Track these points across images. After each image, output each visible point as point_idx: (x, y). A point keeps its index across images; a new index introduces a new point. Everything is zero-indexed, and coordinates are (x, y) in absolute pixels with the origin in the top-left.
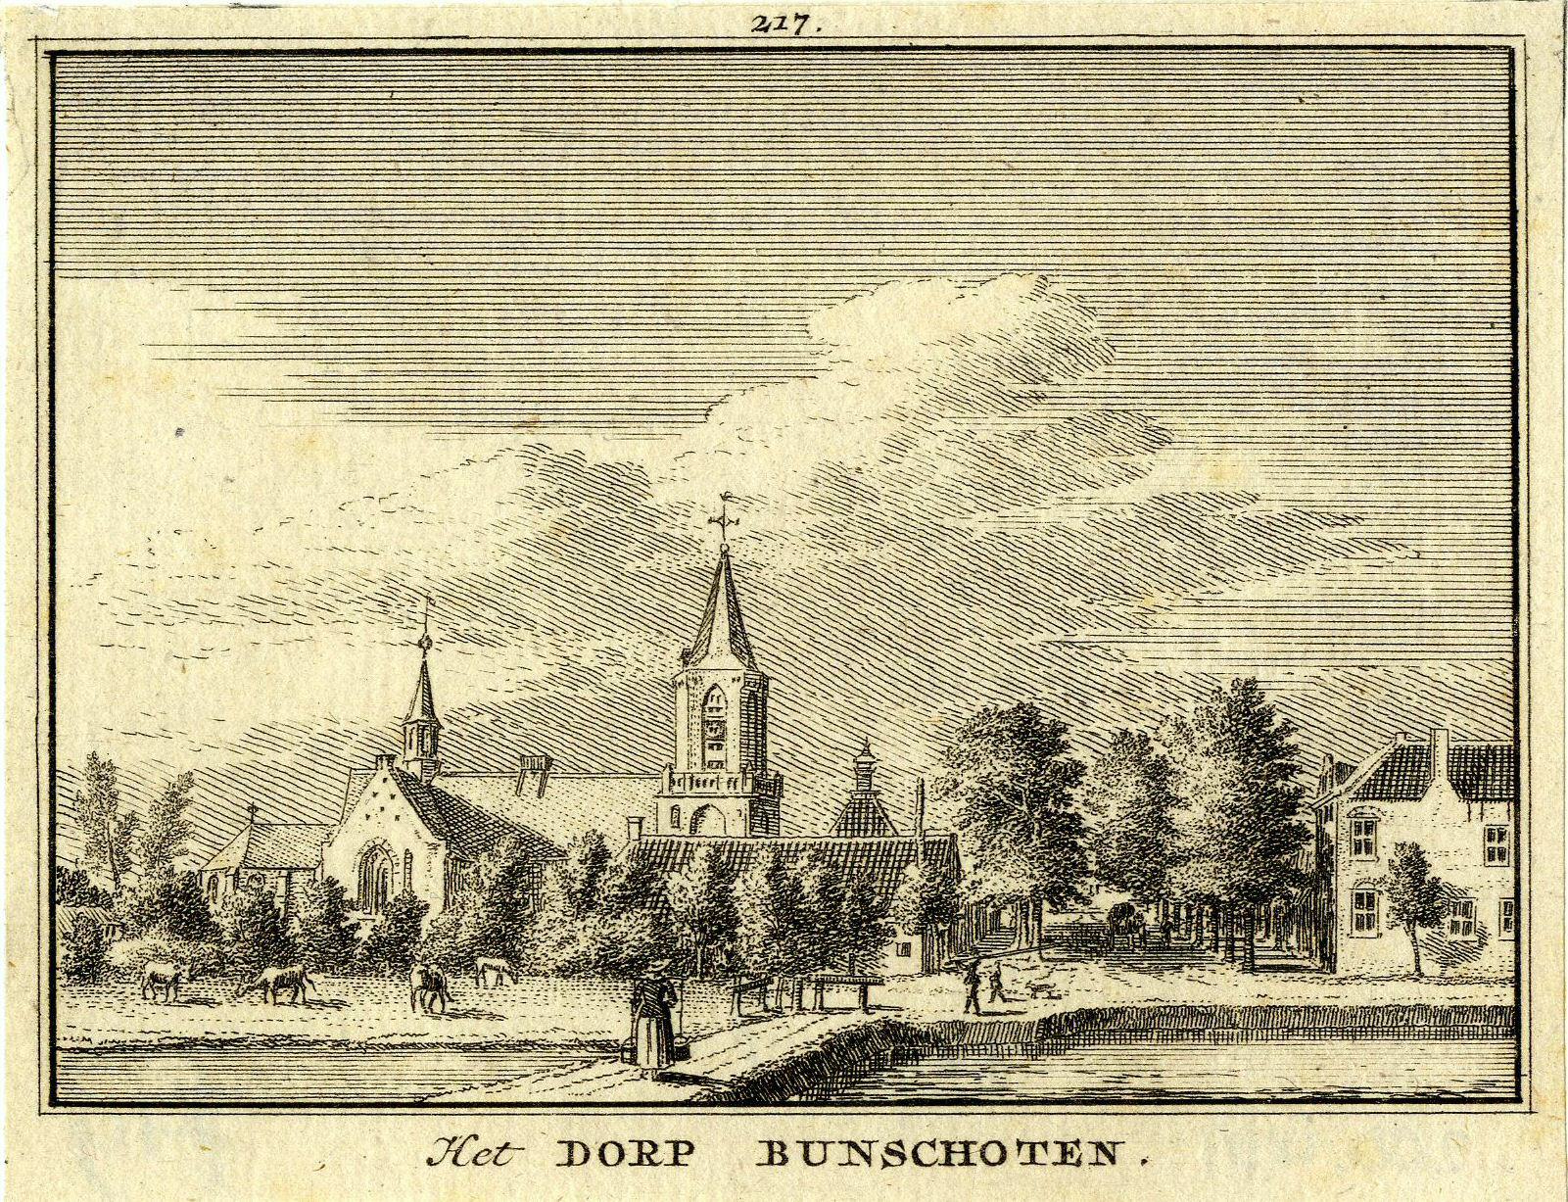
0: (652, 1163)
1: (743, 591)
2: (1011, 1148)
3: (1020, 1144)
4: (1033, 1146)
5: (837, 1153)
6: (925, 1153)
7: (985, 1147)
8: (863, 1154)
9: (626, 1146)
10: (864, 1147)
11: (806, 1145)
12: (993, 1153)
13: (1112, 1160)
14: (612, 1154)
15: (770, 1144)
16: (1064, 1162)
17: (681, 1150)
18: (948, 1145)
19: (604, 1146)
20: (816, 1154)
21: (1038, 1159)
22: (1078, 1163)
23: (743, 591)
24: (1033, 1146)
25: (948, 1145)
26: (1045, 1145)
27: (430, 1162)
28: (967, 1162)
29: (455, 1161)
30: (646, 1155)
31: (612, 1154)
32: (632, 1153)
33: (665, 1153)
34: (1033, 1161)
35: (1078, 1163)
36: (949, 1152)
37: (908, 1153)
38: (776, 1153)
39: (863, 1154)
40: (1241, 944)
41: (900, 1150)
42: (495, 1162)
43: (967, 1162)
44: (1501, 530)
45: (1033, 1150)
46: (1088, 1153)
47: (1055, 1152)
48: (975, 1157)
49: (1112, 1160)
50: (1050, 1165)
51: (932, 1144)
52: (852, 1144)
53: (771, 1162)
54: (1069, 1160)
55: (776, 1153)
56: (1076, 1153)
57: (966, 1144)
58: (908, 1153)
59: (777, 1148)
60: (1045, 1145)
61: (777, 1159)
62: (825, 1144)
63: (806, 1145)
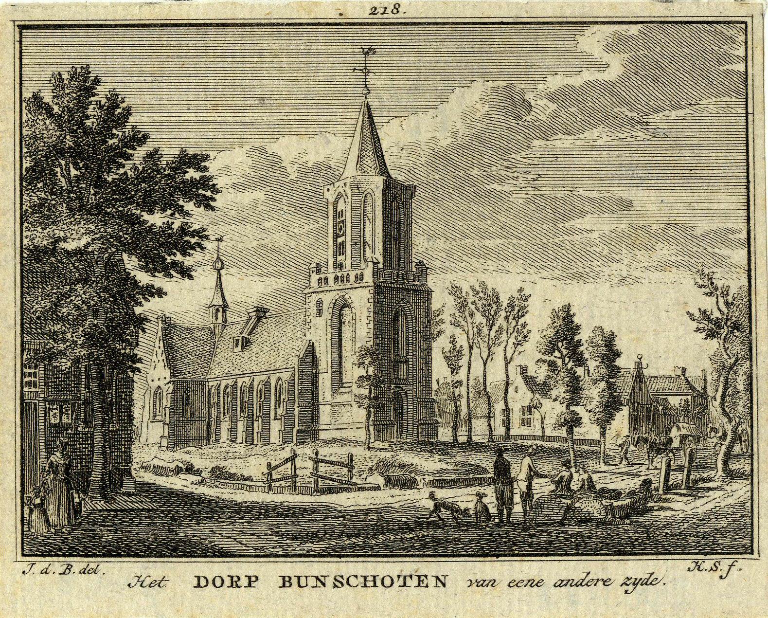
0: (237, 586)
1: (741, 43)
2: (395, 579)
3: (399, 577)
4: (405, 577)
5: (312, 582)
6: (353, 581)
7: (383, 578)
8: (321, 582)
9: (225, 578)
10: (322, 579)
11: (299, 578)
12: (387, 582)
13: (444, 585)
14: (217, 583)
15: (284, 577)
16: (419, 585)
17: (251, 581)
18: (365, 577)
19: (383, 578)
20: (303, 582)
21: (408, 584)
22: (427, 586)
23: (741, 43)
24: (405, 577)
25: (365, 577)
26: (411, 577)
27: (129, 585)
28: (375, 586)
29: (141, 586)
30: (234, 582)
31: (218, 582)
32: (227, 582)
33: (244, 582)
34: (405, 585)
35: (427, 586)
36: (365, 580)
37: (344, 582)
38: (286, 582)
39: (321, 582)
40: (41, 447)
41: (336, 583)
42: (159, 586)
43: (375, 586)
44: (741, 151)
45: (321, 581)
46: (432, 581)
47: (415, 581)
48: (379, 583)
49: (444, 585)
50: (412, 587)
51: (356, 577)
52: (317, 578)
53: (284, 586)
54: (421, 585)
55: (286, 582)
56: (425, 581)
57: (374, 577)
58: (344, 582)
59: (287, 579)
60: (411, 577)
61: (287, 584)
62: (306, 577)
63: (299, 578)
